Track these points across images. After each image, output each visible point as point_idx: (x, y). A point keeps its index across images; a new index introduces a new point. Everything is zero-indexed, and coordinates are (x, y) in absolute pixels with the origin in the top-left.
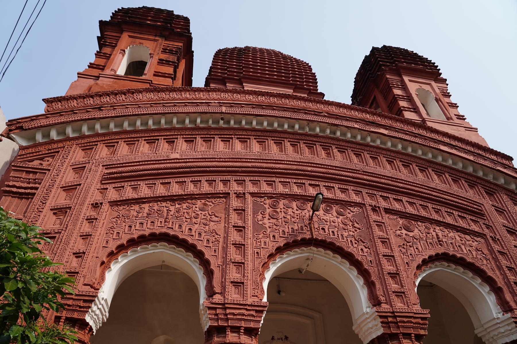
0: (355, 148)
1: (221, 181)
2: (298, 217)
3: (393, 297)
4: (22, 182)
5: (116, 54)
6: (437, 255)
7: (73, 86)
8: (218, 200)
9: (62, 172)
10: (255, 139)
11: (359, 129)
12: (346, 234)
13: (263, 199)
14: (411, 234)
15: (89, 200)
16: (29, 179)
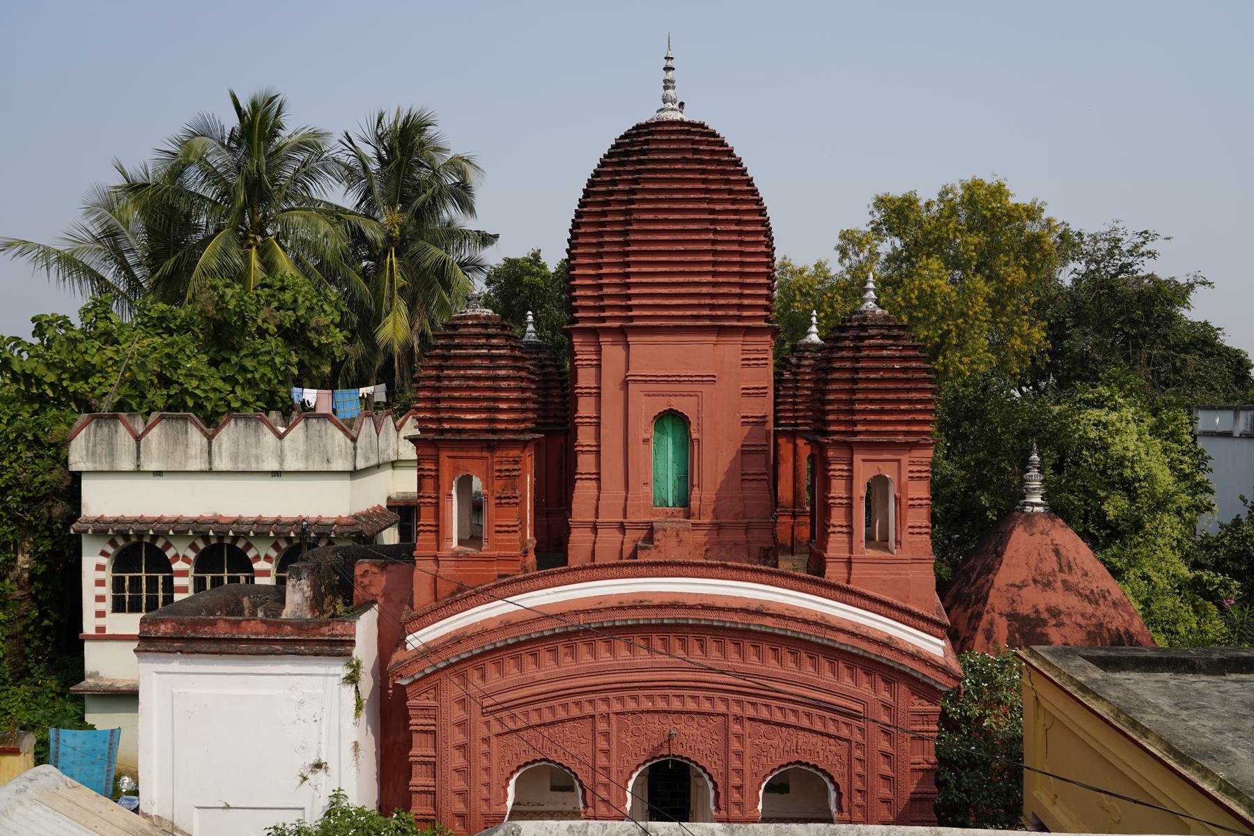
14: (769, 742)
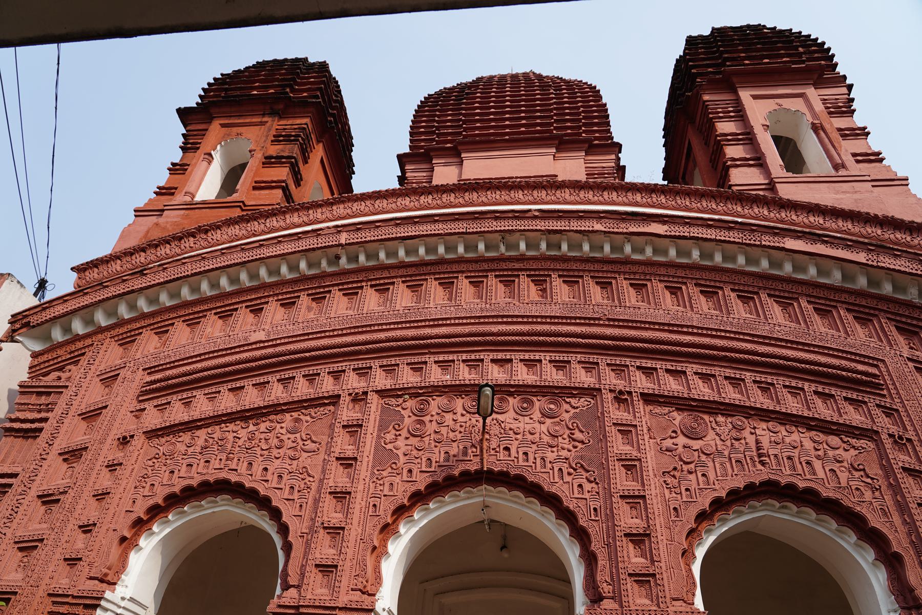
0: (598, 271)
1: (329, 373)
2: (462, 430)
3: (630, 585)
4: (31, 411)
5: (196, 164)
6: (750, 486)
7: (125, 234)
8: (322, 409)
9: (84, 388)
10: (403, 282)
11: (605, 232)
12: (550, 456)
13: (401, 400)
14: (697, 445)
15: (117, 432)
16: (40, 405)
